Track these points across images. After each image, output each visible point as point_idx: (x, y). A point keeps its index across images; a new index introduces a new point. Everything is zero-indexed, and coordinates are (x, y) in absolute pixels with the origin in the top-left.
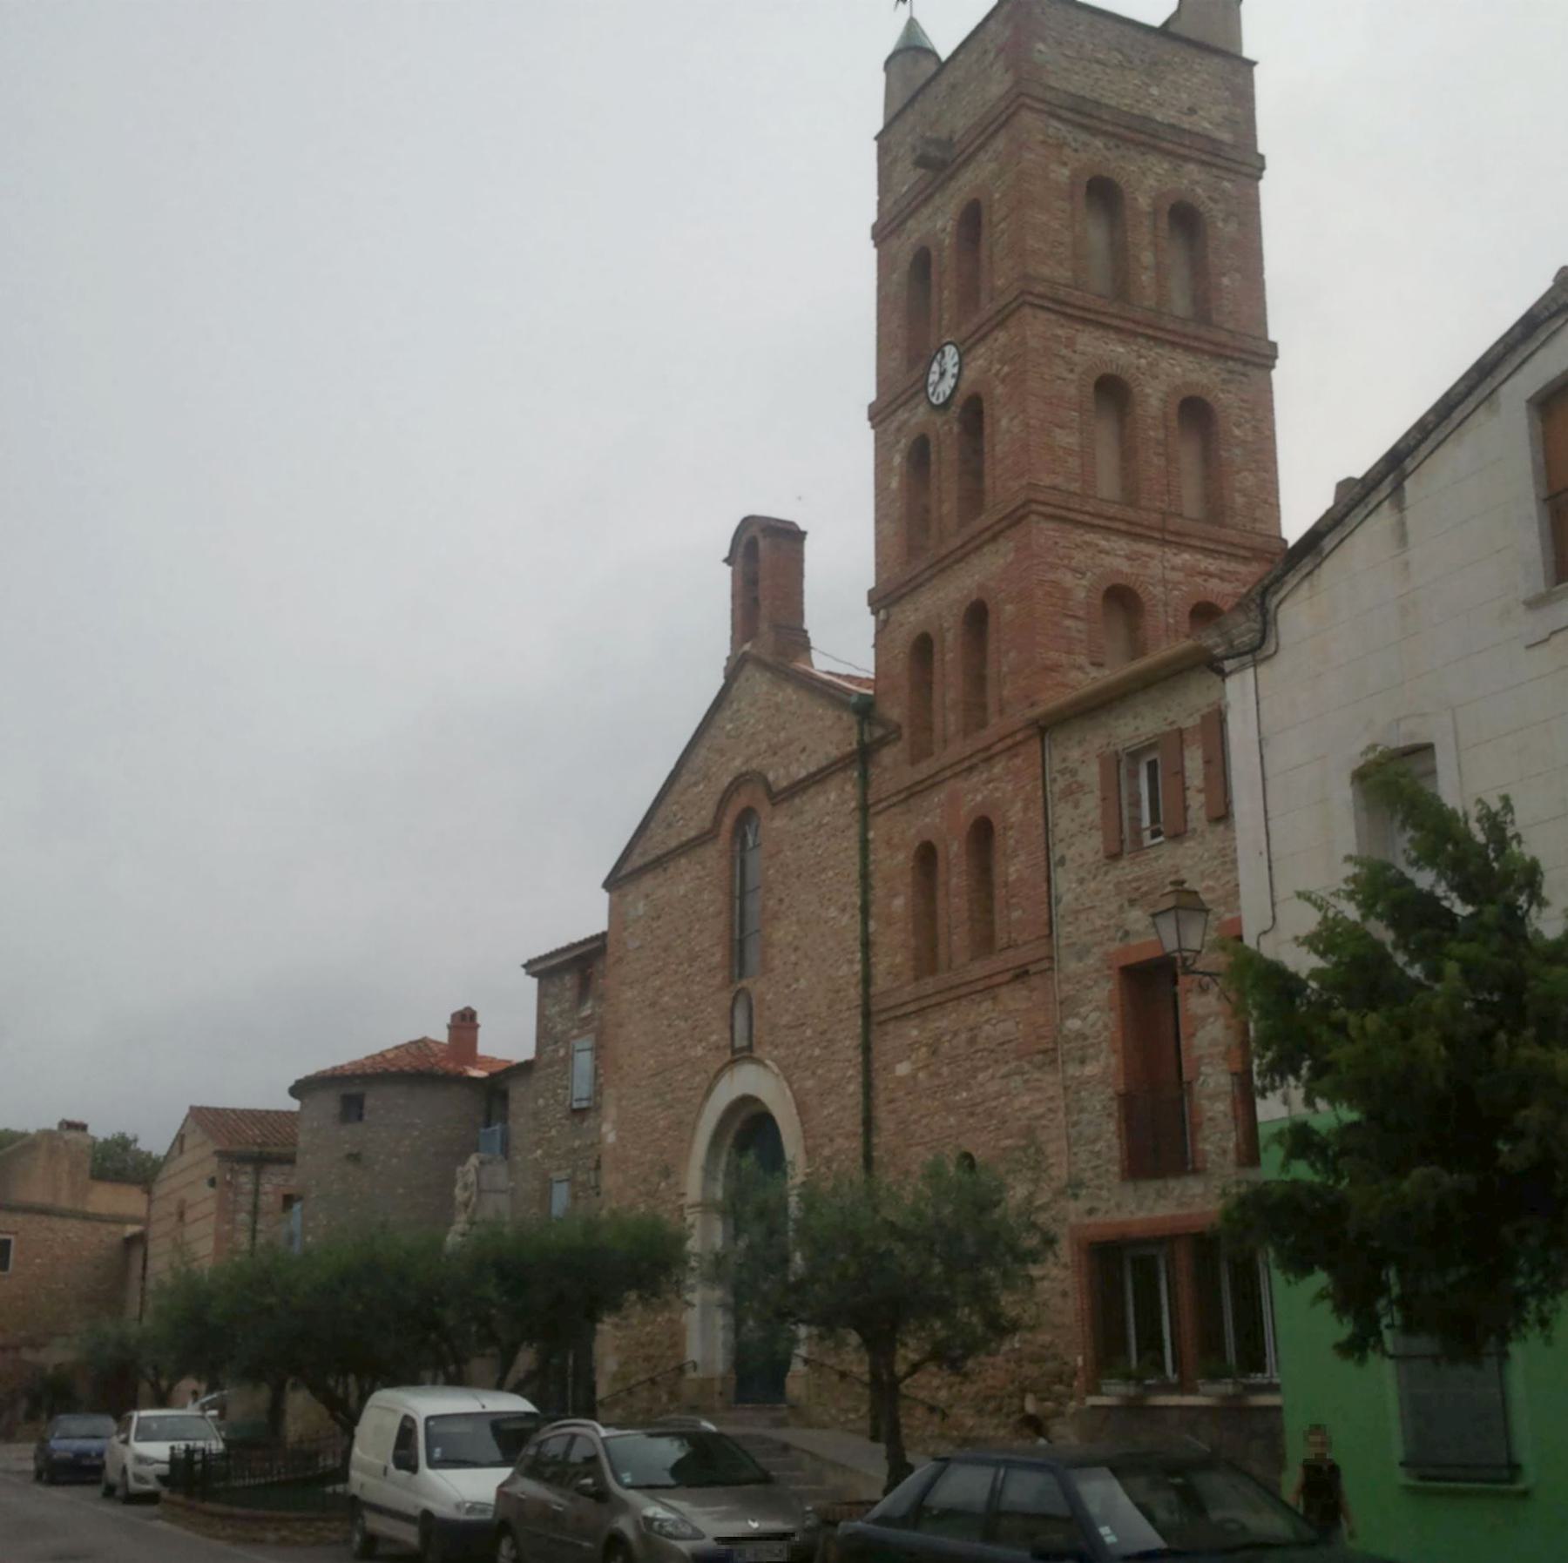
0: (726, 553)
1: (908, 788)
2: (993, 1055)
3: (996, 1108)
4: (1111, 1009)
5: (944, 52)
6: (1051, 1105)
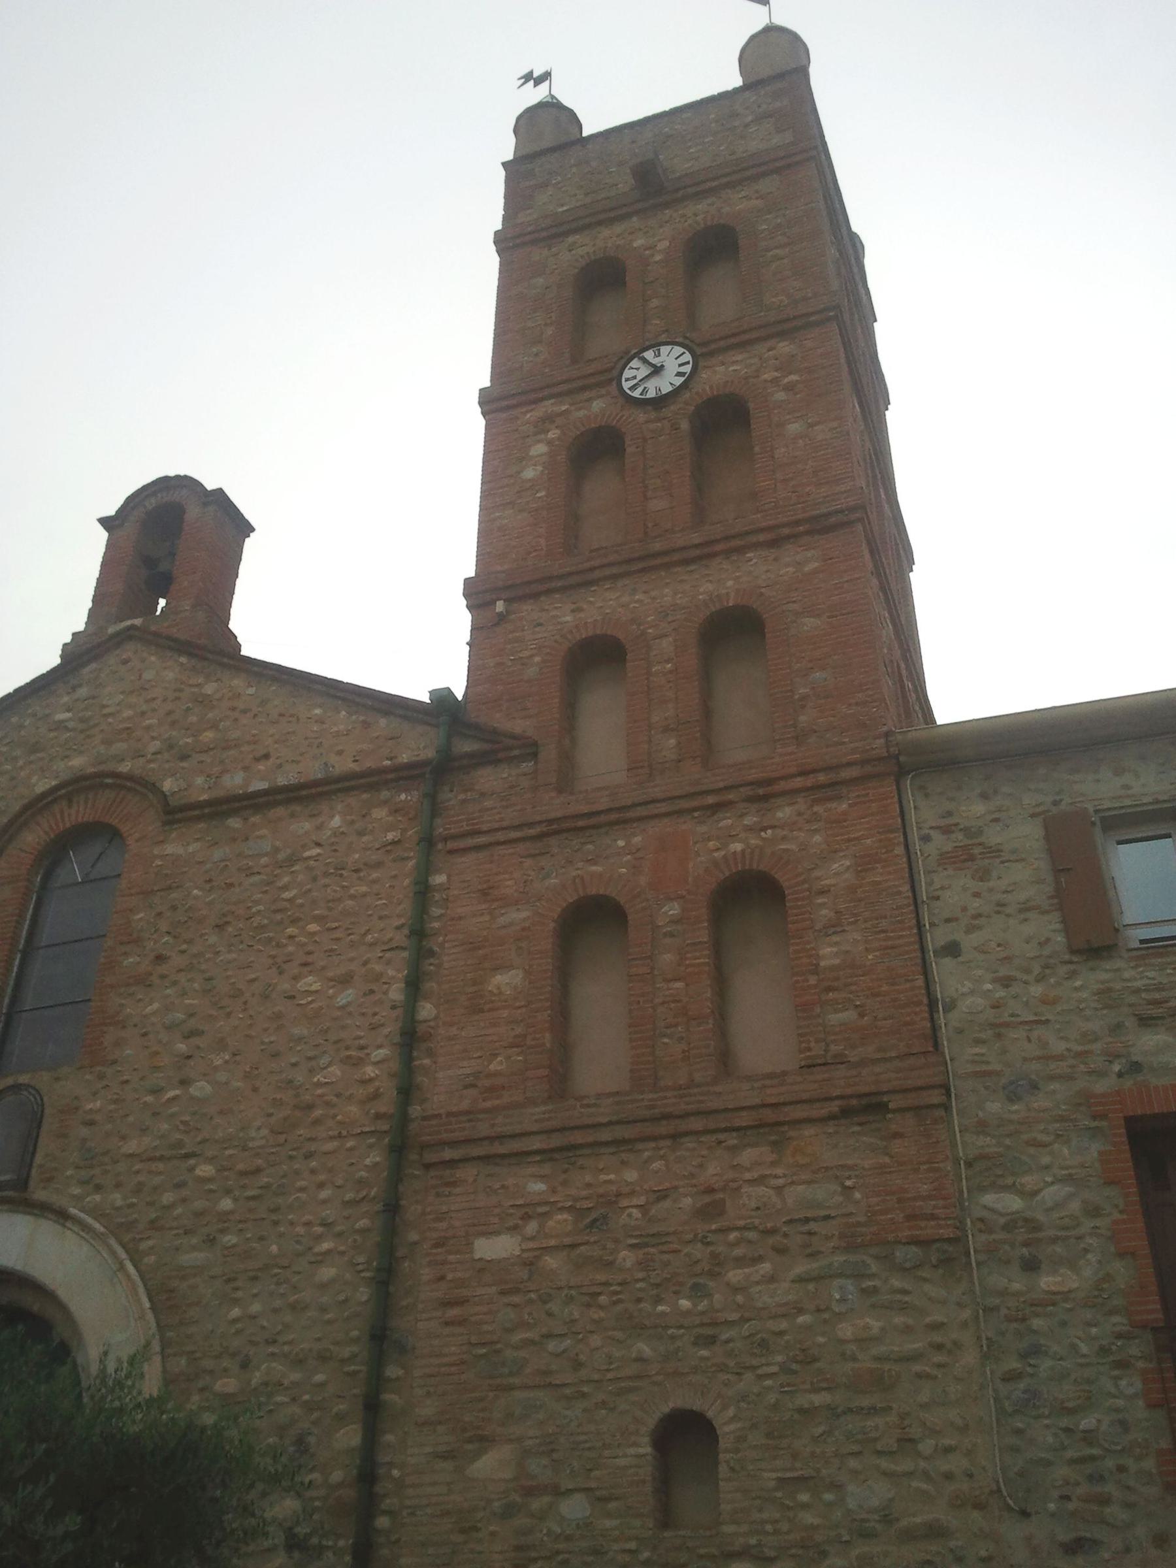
0: (111, 511)
1: (550, 822)
2: (771, 1241)
3: (781, 1333)
4: (1110, 1183)
5: (586, 132)
6: (937, 1338)
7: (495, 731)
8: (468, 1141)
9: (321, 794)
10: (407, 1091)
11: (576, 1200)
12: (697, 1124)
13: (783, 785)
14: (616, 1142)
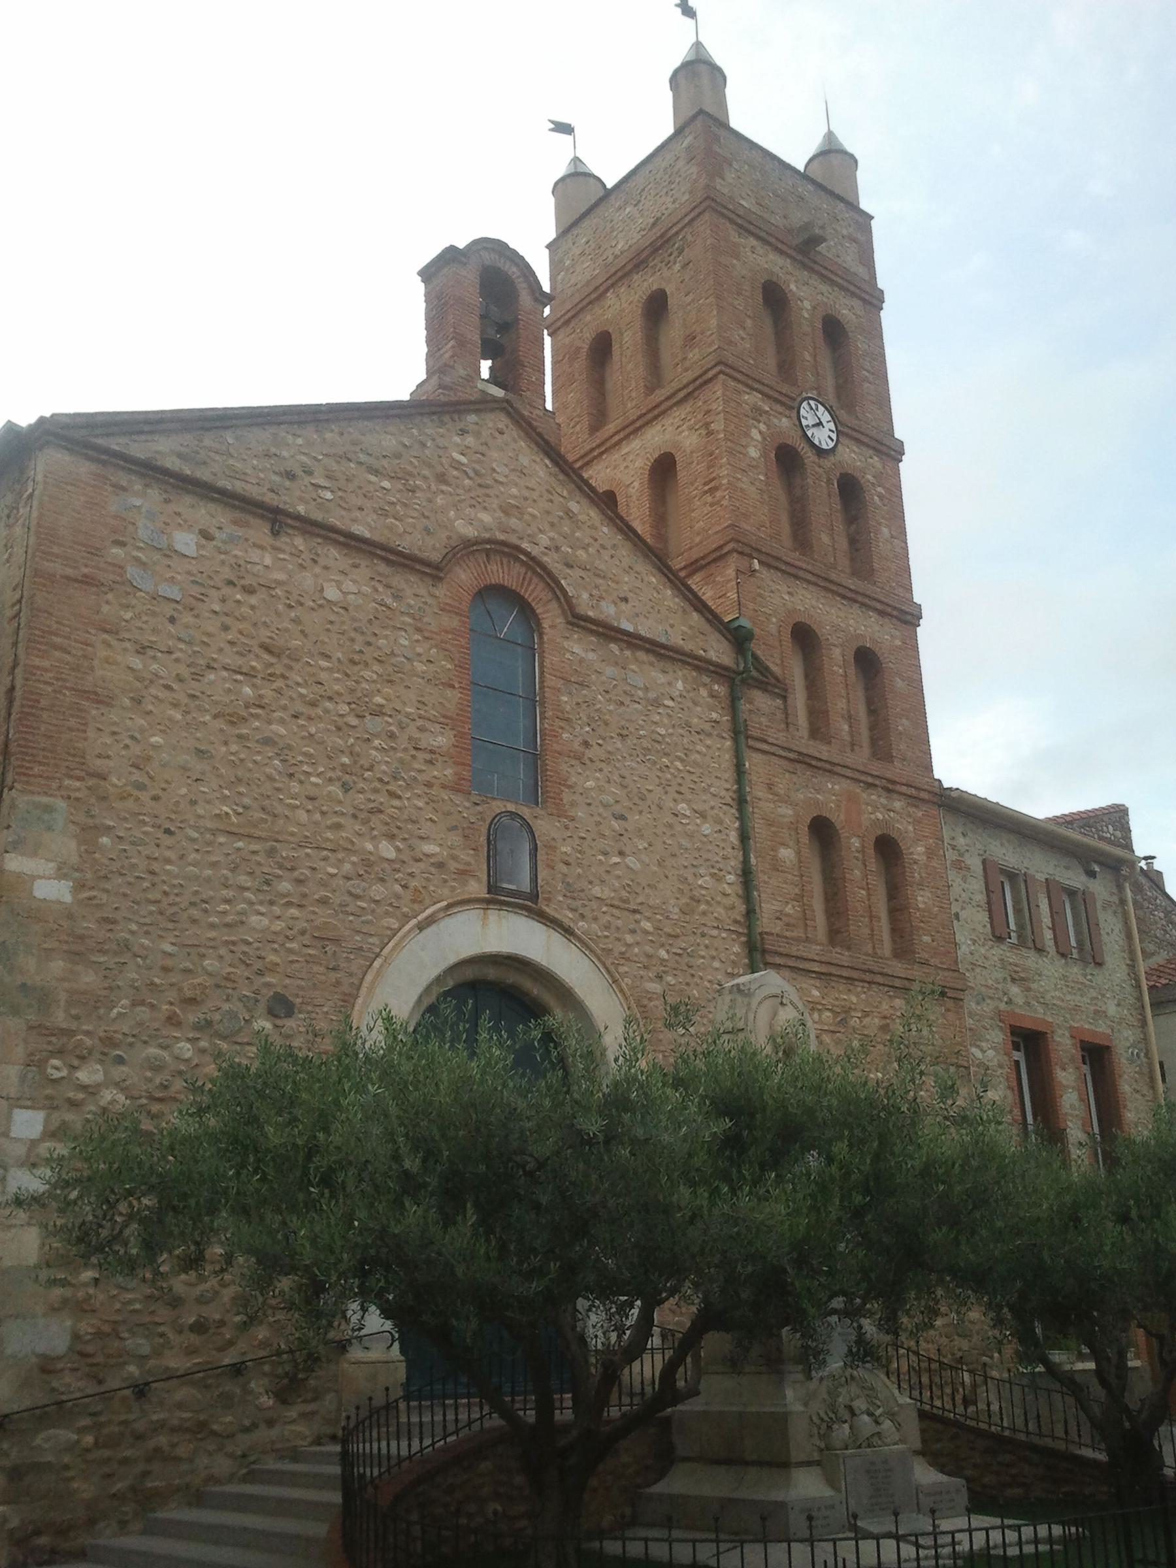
1: (800, 753)
7: (767, 668)
8: (787, 955)
9: (669, 657)
10: (750, 913)
11: (833, 1006)
12: (879, 979)
13: (898, 788)
14: (847, 978)
